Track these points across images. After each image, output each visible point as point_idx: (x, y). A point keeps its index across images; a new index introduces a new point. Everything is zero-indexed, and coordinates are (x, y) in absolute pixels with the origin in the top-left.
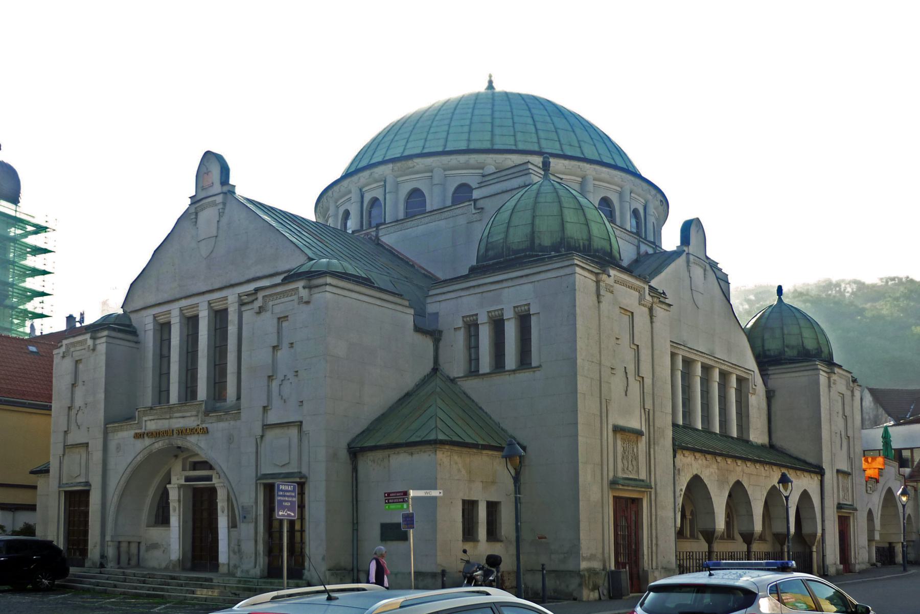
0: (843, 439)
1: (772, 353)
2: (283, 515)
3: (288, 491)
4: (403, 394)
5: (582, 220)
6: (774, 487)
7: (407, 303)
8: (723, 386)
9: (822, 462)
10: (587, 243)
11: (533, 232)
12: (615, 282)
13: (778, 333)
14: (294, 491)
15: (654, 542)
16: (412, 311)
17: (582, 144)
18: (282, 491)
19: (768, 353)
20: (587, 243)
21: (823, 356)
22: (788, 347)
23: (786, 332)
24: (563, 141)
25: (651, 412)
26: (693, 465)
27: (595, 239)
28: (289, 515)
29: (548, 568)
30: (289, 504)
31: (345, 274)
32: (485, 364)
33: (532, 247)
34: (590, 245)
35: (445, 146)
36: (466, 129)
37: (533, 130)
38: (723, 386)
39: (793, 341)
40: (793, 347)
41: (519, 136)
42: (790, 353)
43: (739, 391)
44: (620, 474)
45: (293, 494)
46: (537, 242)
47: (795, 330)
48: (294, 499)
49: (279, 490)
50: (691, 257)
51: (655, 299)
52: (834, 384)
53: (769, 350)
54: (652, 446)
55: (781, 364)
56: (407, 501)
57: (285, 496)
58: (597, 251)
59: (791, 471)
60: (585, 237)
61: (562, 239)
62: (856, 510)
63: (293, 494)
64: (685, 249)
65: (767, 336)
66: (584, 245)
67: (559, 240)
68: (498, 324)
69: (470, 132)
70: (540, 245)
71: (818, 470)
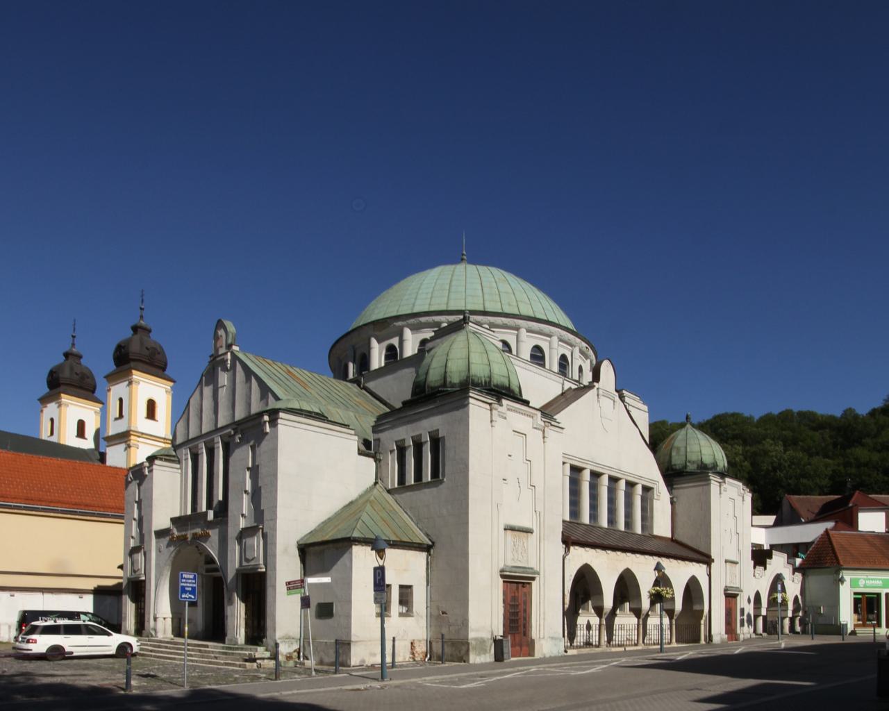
0: (733, 534)
1: (678, 467)
2: (185, 598)
3: (189, 579)
4: (347, 503)
5: (486, 362)
6: (879, 595)
7: (353, 432)
8: (594, 488)
9: (710, 552)
10: (488, 380)
11: (446, 372)
12: (508, 409)
13: (683, 449)
14: (195, 578)
15: (542, 617)
16: (356, 438)
17: (519, 304)
18: (185, 578)
19: (674, 467)
20: (488, 380)
21: (718, 469)
22: (689, 462)
23: (688, 450)
24: (503, 302)
25: (542, 514)
26: (581, 556)
27: (495, 376)
28: (190, 598)
29: (446, 637)
30: (190, 589)
31: (301, 410)
32: (411, 479)
33: (444, 384)
34: (490, 382)
35: (412, 309)
36: (429, 296)
37: (481, 294)
38: (594, 488)
39: (693, 457)
40: (694, 462)
41: (469, 300)
42: (691, 467)
43: (644, 500)
44: (728, 585)
45: (194, 581)
46: (448, 380)
47: (696, 448)
48: (194, 585)
49: (182, 578)
50: (601, 392)
51: (547, 424)
52: (726, 491)
53: (675, 465)
54: (542, 540)
55: (684, 476)
56: (304, 587)
57: (187, 583)
58: (497, 386)
59: (663, 559)
60: (486, 375)
61: (468, 377)
62: (742, 591)
63: (194, 581)
64: (595, 384)
65: (674, 454)
66: (485, 382)
67: (465, 378)
68: (418, 446)
69: (431, 298)
70: (450, 382)
71: (706, 559)
